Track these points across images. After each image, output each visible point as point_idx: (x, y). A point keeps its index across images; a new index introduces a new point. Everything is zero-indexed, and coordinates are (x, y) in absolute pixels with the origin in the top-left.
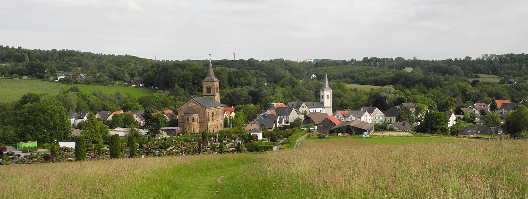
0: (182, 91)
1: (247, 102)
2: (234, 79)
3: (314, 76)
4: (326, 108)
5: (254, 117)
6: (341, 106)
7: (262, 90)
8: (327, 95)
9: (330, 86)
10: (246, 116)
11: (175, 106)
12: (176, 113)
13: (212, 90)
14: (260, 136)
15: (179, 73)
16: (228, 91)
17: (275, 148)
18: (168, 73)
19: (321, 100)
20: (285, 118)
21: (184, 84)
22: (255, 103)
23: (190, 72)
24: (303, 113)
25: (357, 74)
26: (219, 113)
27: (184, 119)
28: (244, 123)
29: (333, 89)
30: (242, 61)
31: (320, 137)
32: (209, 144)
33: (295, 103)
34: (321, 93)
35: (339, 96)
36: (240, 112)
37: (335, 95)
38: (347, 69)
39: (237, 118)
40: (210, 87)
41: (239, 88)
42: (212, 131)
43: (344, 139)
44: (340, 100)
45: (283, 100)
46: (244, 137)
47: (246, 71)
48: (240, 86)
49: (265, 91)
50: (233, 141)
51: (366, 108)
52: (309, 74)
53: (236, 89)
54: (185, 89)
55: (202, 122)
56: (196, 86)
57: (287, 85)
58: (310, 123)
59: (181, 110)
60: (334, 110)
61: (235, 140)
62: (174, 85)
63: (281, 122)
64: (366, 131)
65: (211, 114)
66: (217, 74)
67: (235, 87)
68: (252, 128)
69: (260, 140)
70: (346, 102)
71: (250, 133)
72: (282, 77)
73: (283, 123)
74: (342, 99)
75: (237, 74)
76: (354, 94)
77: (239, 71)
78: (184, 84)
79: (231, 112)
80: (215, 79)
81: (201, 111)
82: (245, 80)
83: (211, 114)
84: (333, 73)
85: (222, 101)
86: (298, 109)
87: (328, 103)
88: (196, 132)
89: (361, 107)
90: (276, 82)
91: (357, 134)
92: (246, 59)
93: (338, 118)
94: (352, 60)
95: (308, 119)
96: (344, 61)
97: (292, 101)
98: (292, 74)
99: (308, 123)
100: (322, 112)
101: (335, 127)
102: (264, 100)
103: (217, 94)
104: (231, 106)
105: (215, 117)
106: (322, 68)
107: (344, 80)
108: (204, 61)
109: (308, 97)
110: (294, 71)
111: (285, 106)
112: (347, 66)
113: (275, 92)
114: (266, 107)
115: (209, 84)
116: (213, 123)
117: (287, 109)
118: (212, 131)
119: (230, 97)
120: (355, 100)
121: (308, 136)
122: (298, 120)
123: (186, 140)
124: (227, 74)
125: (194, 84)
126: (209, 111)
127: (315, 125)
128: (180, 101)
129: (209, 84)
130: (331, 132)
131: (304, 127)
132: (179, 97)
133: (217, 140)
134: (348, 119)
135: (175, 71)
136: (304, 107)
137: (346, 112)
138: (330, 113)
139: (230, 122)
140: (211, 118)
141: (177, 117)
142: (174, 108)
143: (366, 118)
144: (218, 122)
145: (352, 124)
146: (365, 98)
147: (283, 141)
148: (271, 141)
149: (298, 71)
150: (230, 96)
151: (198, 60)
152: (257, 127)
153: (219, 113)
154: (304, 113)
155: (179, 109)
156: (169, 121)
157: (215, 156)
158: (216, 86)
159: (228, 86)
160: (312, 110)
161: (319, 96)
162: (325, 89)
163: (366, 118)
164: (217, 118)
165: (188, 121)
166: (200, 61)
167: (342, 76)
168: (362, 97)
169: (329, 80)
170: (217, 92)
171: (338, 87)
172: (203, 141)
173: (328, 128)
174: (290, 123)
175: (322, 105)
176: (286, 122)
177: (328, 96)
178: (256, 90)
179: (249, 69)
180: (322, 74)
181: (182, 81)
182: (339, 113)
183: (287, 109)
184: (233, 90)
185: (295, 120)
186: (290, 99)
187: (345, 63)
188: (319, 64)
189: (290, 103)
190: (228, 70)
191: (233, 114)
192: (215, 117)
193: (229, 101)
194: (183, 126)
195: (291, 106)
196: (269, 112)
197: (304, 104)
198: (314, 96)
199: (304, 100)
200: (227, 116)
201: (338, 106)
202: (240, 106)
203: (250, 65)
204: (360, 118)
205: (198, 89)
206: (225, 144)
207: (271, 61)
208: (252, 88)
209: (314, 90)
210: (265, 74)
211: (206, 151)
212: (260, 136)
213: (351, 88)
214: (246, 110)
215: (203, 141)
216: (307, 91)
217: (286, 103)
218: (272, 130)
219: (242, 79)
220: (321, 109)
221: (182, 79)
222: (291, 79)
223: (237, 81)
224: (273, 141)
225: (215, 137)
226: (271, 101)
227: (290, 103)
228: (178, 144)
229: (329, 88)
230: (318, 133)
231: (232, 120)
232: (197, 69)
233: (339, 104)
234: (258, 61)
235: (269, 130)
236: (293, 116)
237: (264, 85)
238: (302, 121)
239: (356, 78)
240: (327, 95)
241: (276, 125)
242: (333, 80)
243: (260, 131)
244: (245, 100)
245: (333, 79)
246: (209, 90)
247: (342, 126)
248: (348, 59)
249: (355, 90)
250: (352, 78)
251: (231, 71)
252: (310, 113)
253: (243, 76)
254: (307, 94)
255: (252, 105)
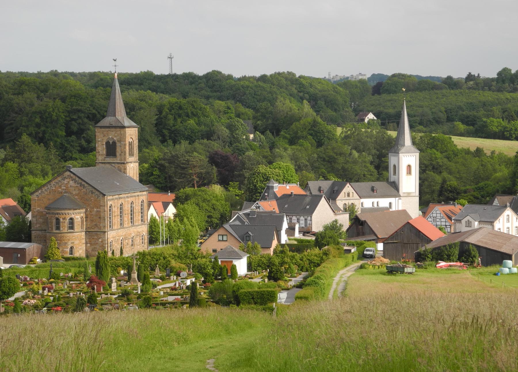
0: (39, 150)
1: (205, 181)
2: (171, 122)
3: (371, 116)
4: (405, 198)
5: (224, 219)
6: (441, 193)
7: (241, 151)
8: (408, 163)
9: (414, 143)
10: (203, 217)
11: (21, 189)
12: (26, 205)
13: (118, 150)
14: (241, 266)
15: (32, 105)
16: (156, 152)
17: (282, 297)
18: (262, 169)
19: (392, 178)
20: (302, 222)
21: (44, 132)
22: (224, 182)
23: (58, 102)
24: (345, 210)
25: (482, 112)
26: (137, 208)
27: (46, 222)
28: (200, 233)
29: (421, 150)
30: (190, 78)
31: (391, 271)
32: (114, 285)
33: (326, 185)
34: (392, 160)
35: (437, 169)
36: (189, 207)
37: (426, 166)
38: (454, 99)
39: (182, 220)
40: (114, 143)
41: (183, 146)
42: (117, 254)
43: (454, 276)
44: (438, 179)
45: (296, 177)
46: (200, 270)
47: (201, 103)
48: (187, 139)
49: (251, 153)
50: (173, 277)
51: (507, 199)
52: (359, 113)
53: (177, 146)
54: (47, 146)
55: (95, 231)
56: (74, 137)
57: (305, 138)
58: (363, 234)
59: (39, 201)
60: (424, 204)
61: (178, 275)
62: (21, 134)
63: (291, 230)
64: (509, 257)
65: (116, 211)
66: (131, 111)
67: (175, 142)
68: (220, 246)
69: (241, 278)
70: (453, 182)
71: (216, 259)
72: (291, 120)
73: (297, 235)
74: (445, 174)
75: (179, 111)
76: (474, 164)
77: (183, 101)
78: (44, 132)
79: (165, 206)
80: (127, 122)
81: (92, 199)
82: (199, 124)
83: (116, 211)
84: (420, 110)
85: (145, 178)
86: (334, 199)
87: (409, 183)
88: (77, 254)
89: (493, 196)
90: (276, 130)
91: (486, 263)
92: (201, 71)
93: (435, 226)
94: (470, 77)
95: (359, 226)
96: (449, 78)
97: (317, 179)
98: (317, 112)
99: (358, 235)
100: (394, 209)
101: (429, 247)
102: (247, 175)
103: (130, 159)
104: (164, 189)
105: (127, 218)
106: (394, 97)
107: (446, 127)
108: (93, 75)
109: (358, 169)
110: (321, 103)
111: (302, 192)
112: (457, 91)
113: (275, 157)
114: (254, 194)
115: (112, 135)
116: (122, 232)
117: (308, 199)
118: (117, 254)
119: (162, 168)
120: (477, 178)
121: (362, 267)
122: (334, 227)
123: (53, 276)
124: (154, 110)
125: (69, 133)
126: (112, 202)
127: (378, 240)
128: (35, 175)
129: (112, 135)
130: (420, 258)
131: (349, 245)
132: (32, 165)
133: (135, 275)
134: (462, 227)
135: (18, 100)
136: (348, 195)
137: (456, 208)
138: (414, 211)
139: (163, 232)
140: (116, 220)
141: (29, 216)
142: (19, 194)
143: (509, 225)
144: (133, 231)
145: (472, 240)
146: (503, 172)
147: (299, 278)
148: (270, 278)
149: (331, 103)
150: (162, 165)
151: (77, 71)
152: (233, 244)
153: (137, 208)
154: (350, 209)
155: (34, 197)
156: (7, 228)
157: (128, 319)
158: (128, 140)
159: (156, 140)
160: (368, 203)
161: (387, 168)
162: (403, 150)
163: (509, 225)
164: (133, 219)
165: (58, 228)
166: (83, 75)
167: (443, 116)
168: (495, 171)
169: (411, 127)
170: (131, 154)
171: (433, 144)
172: (95, 282)
173: (409, 247)
174: (314, 234)
175: (395, 187)
176: (305, 231)
177: (409, 167)
178: (227, 151)
179: (208, 98)
180: (391, 111)
181: (38, 126)
182: (438, 211)
183: (308, 199)
184: (169, 150)
185: (326, 228)
186: (312, 175)
187: (450, 83)
188: (383, 87)
189: (313, 185)
190: (156, 98)
191: (171, 210)
192: (127, 218)
193: (160, 179)
194: (44, 241)
195: (315, 192)
196: (268, 206)
197: (348, 188)
198: (372, 168)
199: (348, 176)
200: (155, 215)
201: (433, 192)
202: (188, 190)
203: (212, 87)
204: (492, 223)
205: (81, 146)
206: (155, 286)
207: (263, 78)
208: (216, 146)
209: (374, 151)
210: (250, 112)
211: (108, 302)
212: (241, 266)
213: (466, 147)
214: (204, 200)
215: (95, 282)
216: (356, 154)
217: (304, 186)
218: (271, 251)
219: (192, 122)
220: (392, 200)
221: (38, 120)
222: (315, 124)
223: (179, 125)
224: (276, 279)
225: (129, 268)
226: (267, 179)
227: (313, 185)
228: (35, 286)
229: (413, 149)
230: (386, 261)
231: (169, 226)
232: (77, 96)
233: (437, 188)
234: (230, 77)
235: (265, 252)
236: (322, 216)
237: (247, 139)
238: (345, 229)
239: (479, 123)
240: (408, 163)
241: (279, 240)
242: (421, 127)
243: (241, 252)
244: (200, 176)
245: (421, 124)
246: (112, 149)
247: (446, 243)
248: (459, 73)
249: (479, 152)
250: (468, 121)
251: (165, 102)
252: (364, 210)
253: (194, 115)
254: (355, 162)
255: (217, 189)
